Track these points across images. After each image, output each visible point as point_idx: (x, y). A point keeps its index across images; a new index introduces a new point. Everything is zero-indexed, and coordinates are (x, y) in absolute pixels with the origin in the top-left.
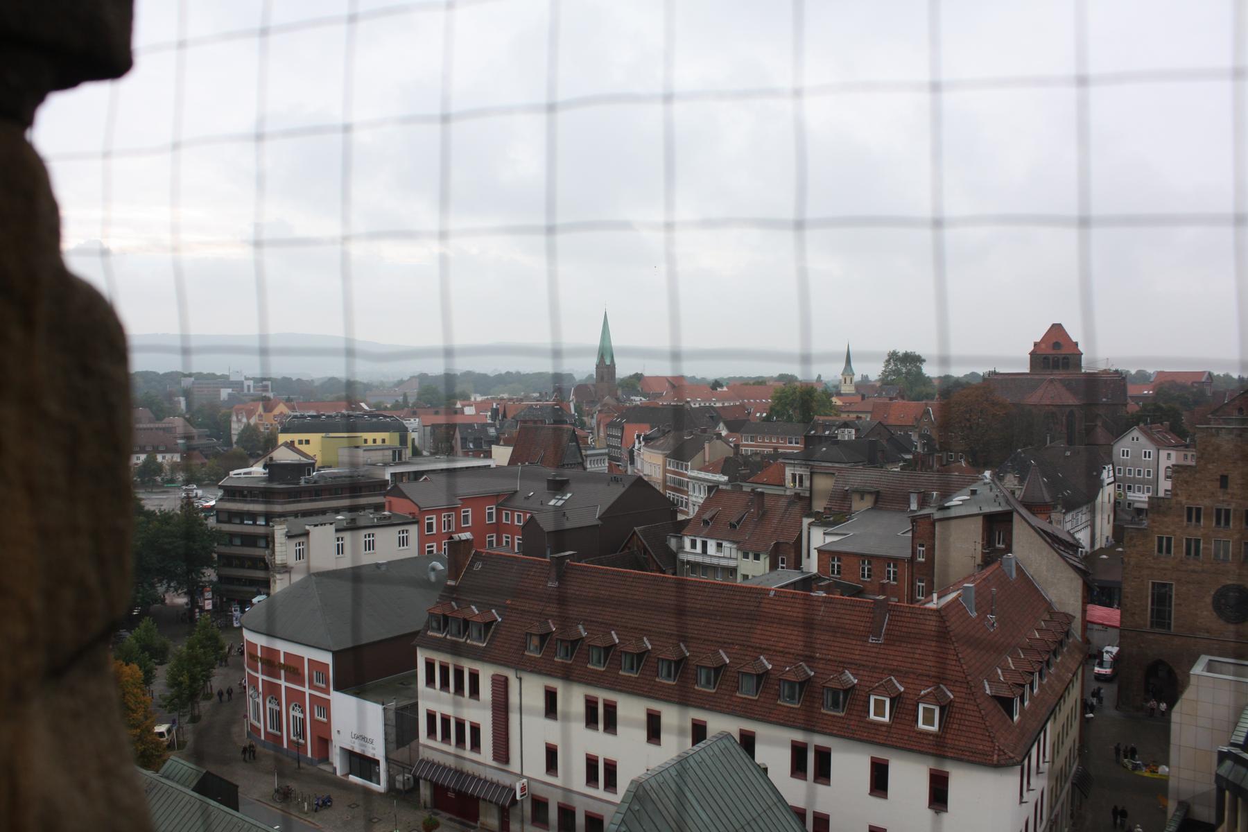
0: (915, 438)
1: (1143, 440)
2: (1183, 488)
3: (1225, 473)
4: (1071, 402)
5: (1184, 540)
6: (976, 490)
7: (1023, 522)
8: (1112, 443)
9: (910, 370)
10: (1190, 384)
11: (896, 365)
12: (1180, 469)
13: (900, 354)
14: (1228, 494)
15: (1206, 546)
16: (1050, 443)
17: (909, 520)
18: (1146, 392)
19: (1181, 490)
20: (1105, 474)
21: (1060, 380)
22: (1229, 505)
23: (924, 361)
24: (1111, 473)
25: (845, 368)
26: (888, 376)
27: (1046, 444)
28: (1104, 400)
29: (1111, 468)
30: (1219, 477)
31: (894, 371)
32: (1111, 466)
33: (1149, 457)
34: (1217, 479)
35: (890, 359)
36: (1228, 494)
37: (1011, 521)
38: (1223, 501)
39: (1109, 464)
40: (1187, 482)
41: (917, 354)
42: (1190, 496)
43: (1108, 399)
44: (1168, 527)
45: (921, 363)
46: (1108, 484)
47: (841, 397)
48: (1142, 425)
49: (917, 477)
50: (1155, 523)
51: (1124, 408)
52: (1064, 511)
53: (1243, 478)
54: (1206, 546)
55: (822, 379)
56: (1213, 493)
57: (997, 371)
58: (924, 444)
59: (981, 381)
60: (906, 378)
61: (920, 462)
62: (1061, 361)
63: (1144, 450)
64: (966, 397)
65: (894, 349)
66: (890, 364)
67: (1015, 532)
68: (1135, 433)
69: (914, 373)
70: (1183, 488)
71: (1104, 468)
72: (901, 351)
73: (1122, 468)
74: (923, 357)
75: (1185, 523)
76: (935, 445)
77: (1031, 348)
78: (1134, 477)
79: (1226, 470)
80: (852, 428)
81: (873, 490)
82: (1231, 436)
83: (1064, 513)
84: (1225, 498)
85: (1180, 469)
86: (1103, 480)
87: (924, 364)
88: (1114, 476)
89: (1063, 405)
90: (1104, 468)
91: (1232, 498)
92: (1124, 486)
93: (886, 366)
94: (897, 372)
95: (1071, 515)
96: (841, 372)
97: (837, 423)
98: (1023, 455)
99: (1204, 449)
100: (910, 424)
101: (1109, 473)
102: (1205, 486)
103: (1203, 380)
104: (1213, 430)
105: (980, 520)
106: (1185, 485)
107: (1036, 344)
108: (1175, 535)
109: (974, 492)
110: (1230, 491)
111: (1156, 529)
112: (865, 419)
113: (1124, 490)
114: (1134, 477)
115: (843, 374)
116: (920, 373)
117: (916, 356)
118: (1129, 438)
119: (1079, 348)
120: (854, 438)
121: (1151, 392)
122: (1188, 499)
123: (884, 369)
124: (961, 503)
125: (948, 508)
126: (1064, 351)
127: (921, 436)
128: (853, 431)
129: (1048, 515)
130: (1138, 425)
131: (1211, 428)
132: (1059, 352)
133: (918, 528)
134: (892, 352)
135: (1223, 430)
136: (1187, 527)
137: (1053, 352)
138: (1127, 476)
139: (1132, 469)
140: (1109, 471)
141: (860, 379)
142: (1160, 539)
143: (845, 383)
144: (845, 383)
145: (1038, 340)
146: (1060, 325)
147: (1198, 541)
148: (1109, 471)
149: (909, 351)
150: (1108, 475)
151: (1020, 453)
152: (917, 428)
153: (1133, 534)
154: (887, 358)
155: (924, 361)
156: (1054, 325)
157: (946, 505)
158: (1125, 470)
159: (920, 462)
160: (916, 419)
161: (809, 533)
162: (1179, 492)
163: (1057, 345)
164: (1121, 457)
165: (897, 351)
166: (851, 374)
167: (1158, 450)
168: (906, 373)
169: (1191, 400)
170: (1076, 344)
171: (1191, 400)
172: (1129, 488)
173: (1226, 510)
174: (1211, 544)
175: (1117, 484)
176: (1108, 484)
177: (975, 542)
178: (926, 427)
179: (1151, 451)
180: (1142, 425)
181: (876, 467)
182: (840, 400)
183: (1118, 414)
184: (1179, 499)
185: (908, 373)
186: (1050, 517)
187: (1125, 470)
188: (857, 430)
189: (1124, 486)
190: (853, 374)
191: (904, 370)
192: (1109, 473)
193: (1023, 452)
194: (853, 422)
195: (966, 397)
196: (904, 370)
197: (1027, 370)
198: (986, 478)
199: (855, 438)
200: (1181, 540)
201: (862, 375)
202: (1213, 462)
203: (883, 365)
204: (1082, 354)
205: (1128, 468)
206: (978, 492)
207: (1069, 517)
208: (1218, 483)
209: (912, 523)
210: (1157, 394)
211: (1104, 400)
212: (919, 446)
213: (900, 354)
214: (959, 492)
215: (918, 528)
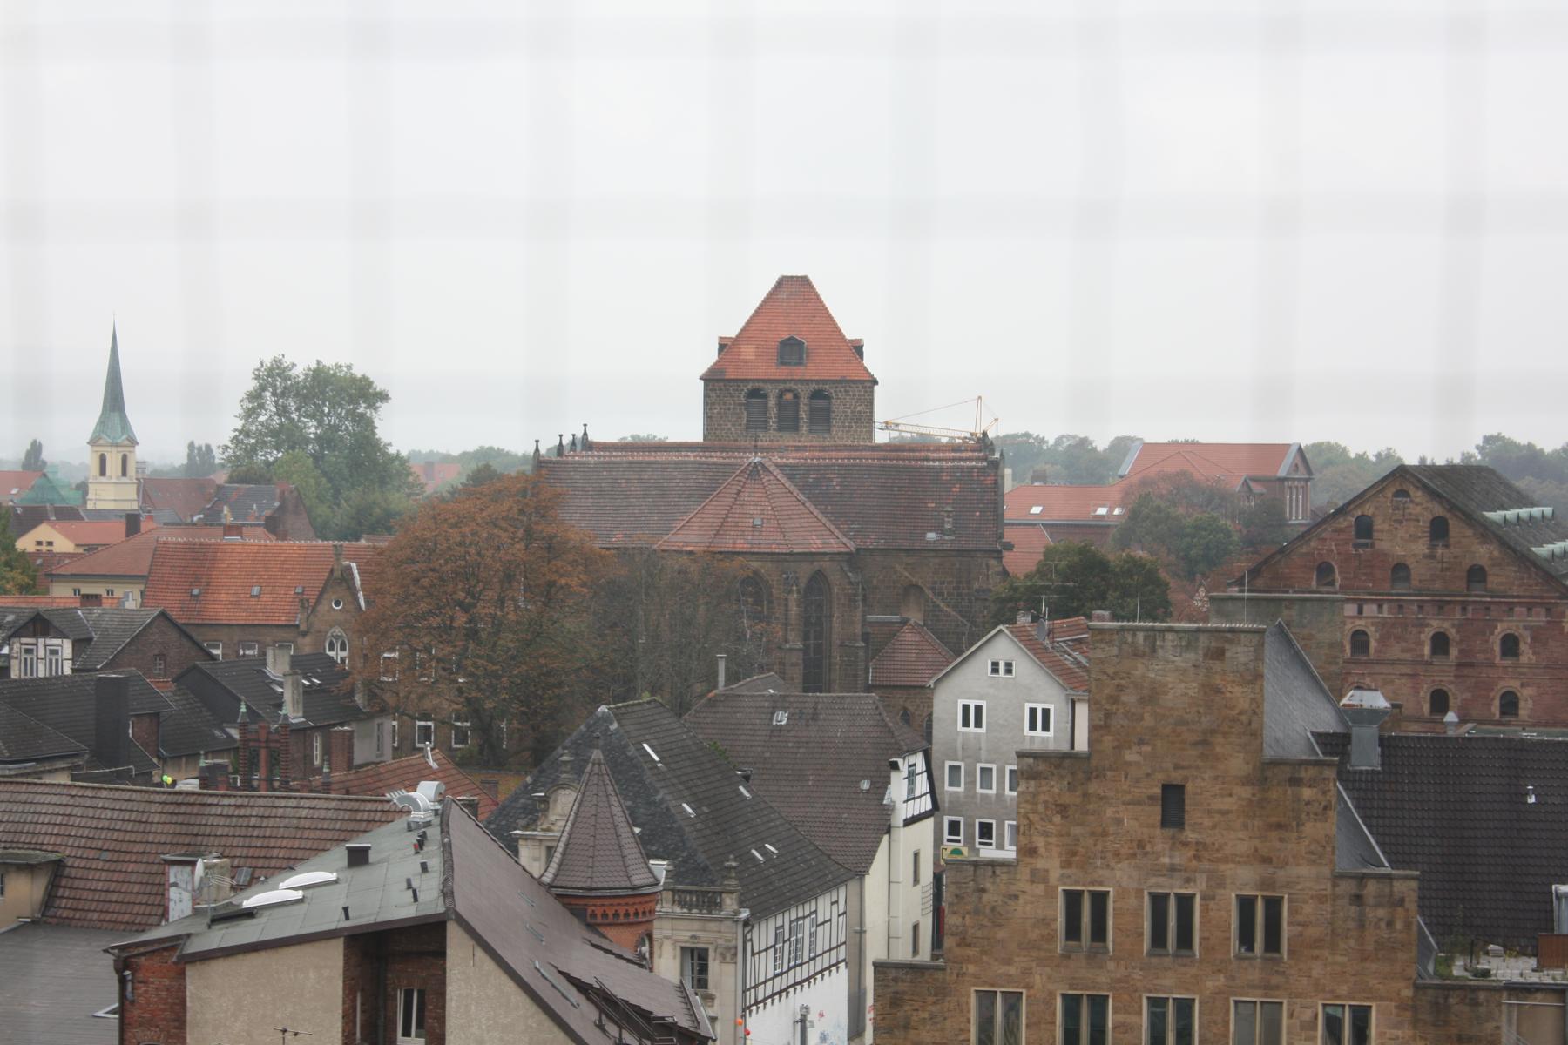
0: (277, 667)
1: (1026, 669)
2: (1051, 828)
3: (1176, 777)
4: (815, 543)
5: (1059, 1002)
6: (368, 849)
7: (480, 953)
8: (931, 683)
9: (336, 428)
10: (1237, 485)
11: (283, 411)
12: (1042, 767)
13: (299, 372)
14: (1185, 844)
15: (1121, 1017)
16: (728, 681)
17: (109, 960)
18: (1102, 511)
19: (1046, 834)
20: (897, 788)
21: (791, 472)
22: (1188, 880)
23: (383, 397)
24: (922, 784)
25: (103, 422)
26: (252, 451)
27: (715, 687)
28: (931, 536)
29: (921, 765)
30: (1158, 791)
31: (275, 433)
32: (919, 761)
33: (1046, 728)
34: (1151, 798)
35: (263, 388)
36: (1185, 844)
37: (441, 954)
38: (1173, 869)
39: (913, 752)
40: (1063, 809)
41: (358, 372)
42: (1074, 854)
43: (943, 532)
44: (1009, 962)
45: (371, 406)
46: (909, 822)
47: (74, 525)
48: (1023, 620)
49: (195, 810)
50: (969, 945)
51: (993, 562)
52: (745, 914)
53: (440, 802)
54: (1121, 1017)
55: (46, 455)
56: (1141, 845)
57: (594, 437)
58: (308, 692)
59: (528, 468)
60: (317, 458)
61: (263, 754)
62: (804, 400)
63: (1028, 706)
64: (456, 525)
65: (277, 354)
66: (262, 406)
67: (454, 989)
68: (1003, 647)
69: (348, 440)
70: (1051, 828)
71: (895, 766)
72: (301, 364)
73: (962, 764)
74: (379, 385)
75: (1060, 944)
76: (351, 693)
77: (710, 357)
78: (1000, 795)
79: (1177, 767)
80: (64, 636)
81: (39, 856)
82: (1191, 656)
83: (746, 923)
84: (1177, 861)
85: (1042, 767)
86: (888, 810)
87: (384, 408)
88: (932, 792)
89: (791, 554)
90: (895, 766)
91: (1197, 857)
92: (970, 826)
93: (249, 414)
94: (287, 436)
95: (772, 925)
96: (88, 436)
97: (10, 618)
98: (614, 726)
99: (1114, 700)
100: (283, 621)
101: (911, 782)
102: (1119, 822)
103: (1282, 472)
104: (1140, 636)
105: (335, 953)
106: (1057, 819)
107: (723, 346)
108: (1028, 987)
109: (358, 858)
110: (1190, 835)
111: (971, 969)
112: (120, 601)
113: (969, 841)
114: (1000, 795)
115: (93, 442)
116: (366, 442)
117: (353, 379)
118: (982, 662)
119: (867, 362)
120: (67, 671)
121: (1117, 512)
122: (1066, 864)
123: (239, 424)
124: (299, 894)
125: (250, 914)
126: (814, 370)
127: (300, 665)
128: (67, 648)
129: (641, 930)
130: (1011, 621)
131: (1134, 630)
132: (800, 373)
133: (142, 989)
134: (268, 362)
135: (1169, 636)
136: (1066, 956)
137: (782, 373)
138: (979, 790)
139: (994, 767)
140: (911, 776)
141: (185, 461)
142: (987, 998)
143: (103, 472)
144: (103, 472)
145: (732, 331)
146: (804, 281)
147: (1099, 1004)
148: (911, 776)
149: (329, 362)
150: (911, 791)
151: (606, 719)
152: (304, 634)
153: (901, 987)
154: (252, 385)
155: (383, 397)
156: (783, 282)
157: (247, 904)
158: (970, 774)
159: (263, 754)
160: (303, 603)
161: (682, 974)
162: (1040, 842)
163: (791, 350)
164: (960, 728)
165: (287, 362)
166: (123, 439)
167: (1073, 703)
168: (318, 438)
169: (1236, 537)
170: (857, 348)
171: (1236, 537)
172: (986, 831)
173: (1179, 897)
174: (1140, 1013)
175: (946, 819)
176: (909, 822)
177: (284, 1031)
178: (338, 631)
179: (1052, 707)
180: (1023, 620)
181: (120, 777)
182: (67, 535)
183: (976, 585)
184: (1040, 864)
185: (327, 440)
186: (650, 936)
187: (970, 774)
188: (81, 644)
189: (970, 826)
190: (133, 442)
191: (312, 429)
192: (911, 782)
193: (619, 715)
194: (65, 612)
195: (456, 525)
196: (312, 429)
197: (693, 431)
198: (418, 809)
199: (74, 670)
200: (1050, 1003)
201: (191, 445)
202: (1141, 742)
203: (239, 411)
204: (875, 382)
205: (979, 766)
206: (372, 857)
207: (763, 935)
208: (1157, 810)
209: (119, 971)
210: (1134, 516)
211: (931, 536)
212: (288, 697)
213: (299, 372)
214: (316, 860)
215: (142, 989)
